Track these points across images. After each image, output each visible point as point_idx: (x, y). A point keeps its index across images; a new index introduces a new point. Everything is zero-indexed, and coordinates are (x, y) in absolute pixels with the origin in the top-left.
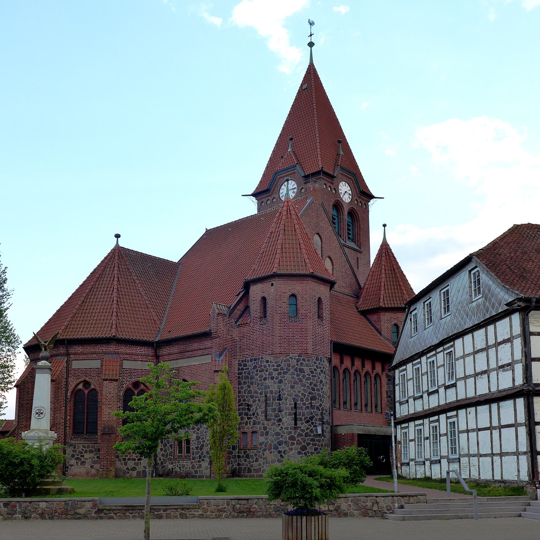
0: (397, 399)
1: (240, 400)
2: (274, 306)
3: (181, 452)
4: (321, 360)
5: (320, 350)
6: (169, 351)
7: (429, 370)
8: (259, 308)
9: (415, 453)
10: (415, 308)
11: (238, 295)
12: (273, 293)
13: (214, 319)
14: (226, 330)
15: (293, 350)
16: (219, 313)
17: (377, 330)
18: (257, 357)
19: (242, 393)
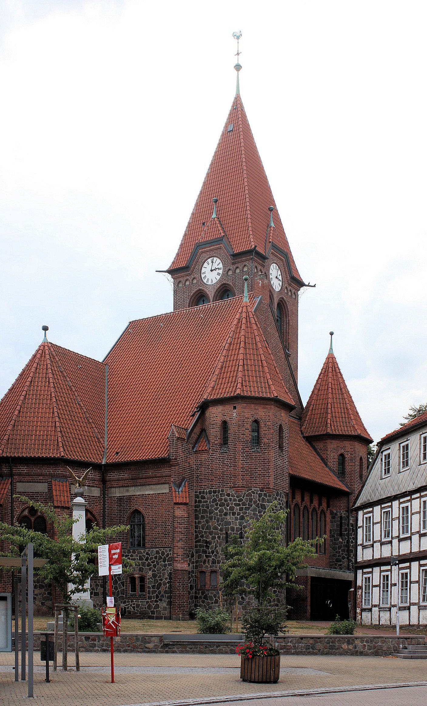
0: (360, 541)
1: (197, 536)
2: (237, 433)
3: (134, 589)
4: (280, 496)
5: (280, 485)
6: (118, 476)
7: (401, 515)
8: (219, 433)
9: (380, 599)
10: (388, 448)
11: (193, 415)
12: (235, 418)
13: (173, 443)
14: (184, 456)
15: (255, 483)
16: (179, 438)
17: (323, 459)
18: (217, 489)
19: (200, 529)
